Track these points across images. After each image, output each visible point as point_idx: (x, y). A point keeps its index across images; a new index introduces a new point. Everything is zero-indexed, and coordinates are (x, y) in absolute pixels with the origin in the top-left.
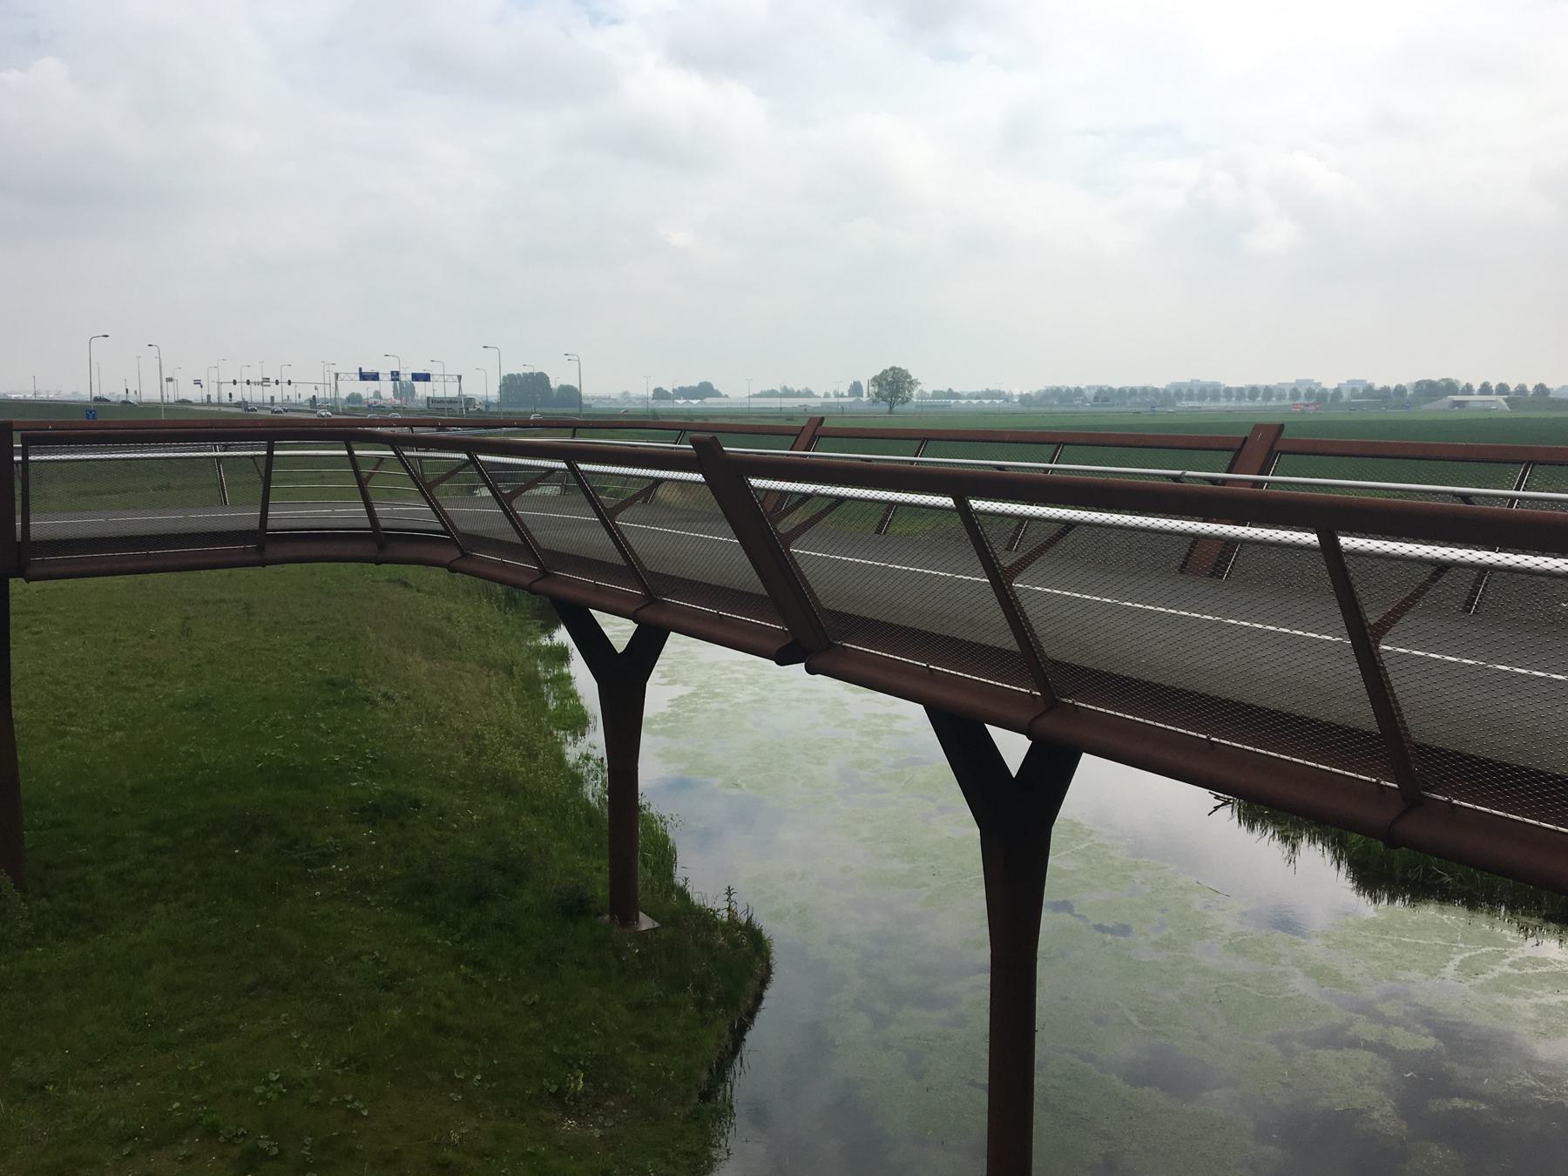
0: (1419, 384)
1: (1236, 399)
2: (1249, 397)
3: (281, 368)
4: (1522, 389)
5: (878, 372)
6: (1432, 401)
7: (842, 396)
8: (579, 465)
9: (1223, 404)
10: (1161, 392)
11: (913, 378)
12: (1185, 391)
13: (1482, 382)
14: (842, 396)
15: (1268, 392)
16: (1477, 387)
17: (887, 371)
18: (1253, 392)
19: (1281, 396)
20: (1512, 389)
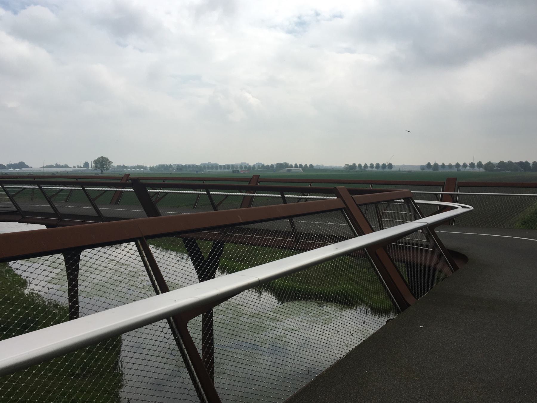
0: (277, 164)
7: (81, 167)
11: (110, 161)
12: (206, 166)
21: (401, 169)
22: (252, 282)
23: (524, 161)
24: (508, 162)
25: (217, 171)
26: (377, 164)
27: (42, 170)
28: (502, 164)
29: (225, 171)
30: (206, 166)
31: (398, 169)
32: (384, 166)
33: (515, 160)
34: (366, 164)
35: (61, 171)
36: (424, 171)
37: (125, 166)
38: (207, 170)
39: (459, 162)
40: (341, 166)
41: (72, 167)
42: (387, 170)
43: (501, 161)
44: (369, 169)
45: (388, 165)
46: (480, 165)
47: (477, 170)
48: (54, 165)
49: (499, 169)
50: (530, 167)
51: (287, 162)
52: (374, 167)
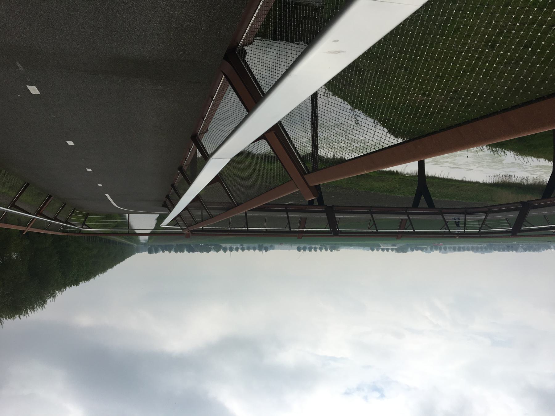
0: (406, 252)
1: (465, 247)
2: (461, 248)
4: (378, 250)
6: (402, 246)
8: (23, 234)
9: (470, 246)
10: (493, 250)
13: (389, 252)
15: (454, 249)
16: (390, 251)
18: (459, 250)
19: (450, 248)
20: (380, 250)
24: (203, 252)
26: (260, 251)
28: (208, 251)
31: (292, 246)
32: (305, 249)
36: (270, 245)
39: (242, 252)
42: (302, 246)
43: (189, 253)
44: (318, 246)
46: (225, 250)
47: (228, 246)
49: (210, 246)
50: (186, 248)
51: (397, 253)
52: (314, 248)
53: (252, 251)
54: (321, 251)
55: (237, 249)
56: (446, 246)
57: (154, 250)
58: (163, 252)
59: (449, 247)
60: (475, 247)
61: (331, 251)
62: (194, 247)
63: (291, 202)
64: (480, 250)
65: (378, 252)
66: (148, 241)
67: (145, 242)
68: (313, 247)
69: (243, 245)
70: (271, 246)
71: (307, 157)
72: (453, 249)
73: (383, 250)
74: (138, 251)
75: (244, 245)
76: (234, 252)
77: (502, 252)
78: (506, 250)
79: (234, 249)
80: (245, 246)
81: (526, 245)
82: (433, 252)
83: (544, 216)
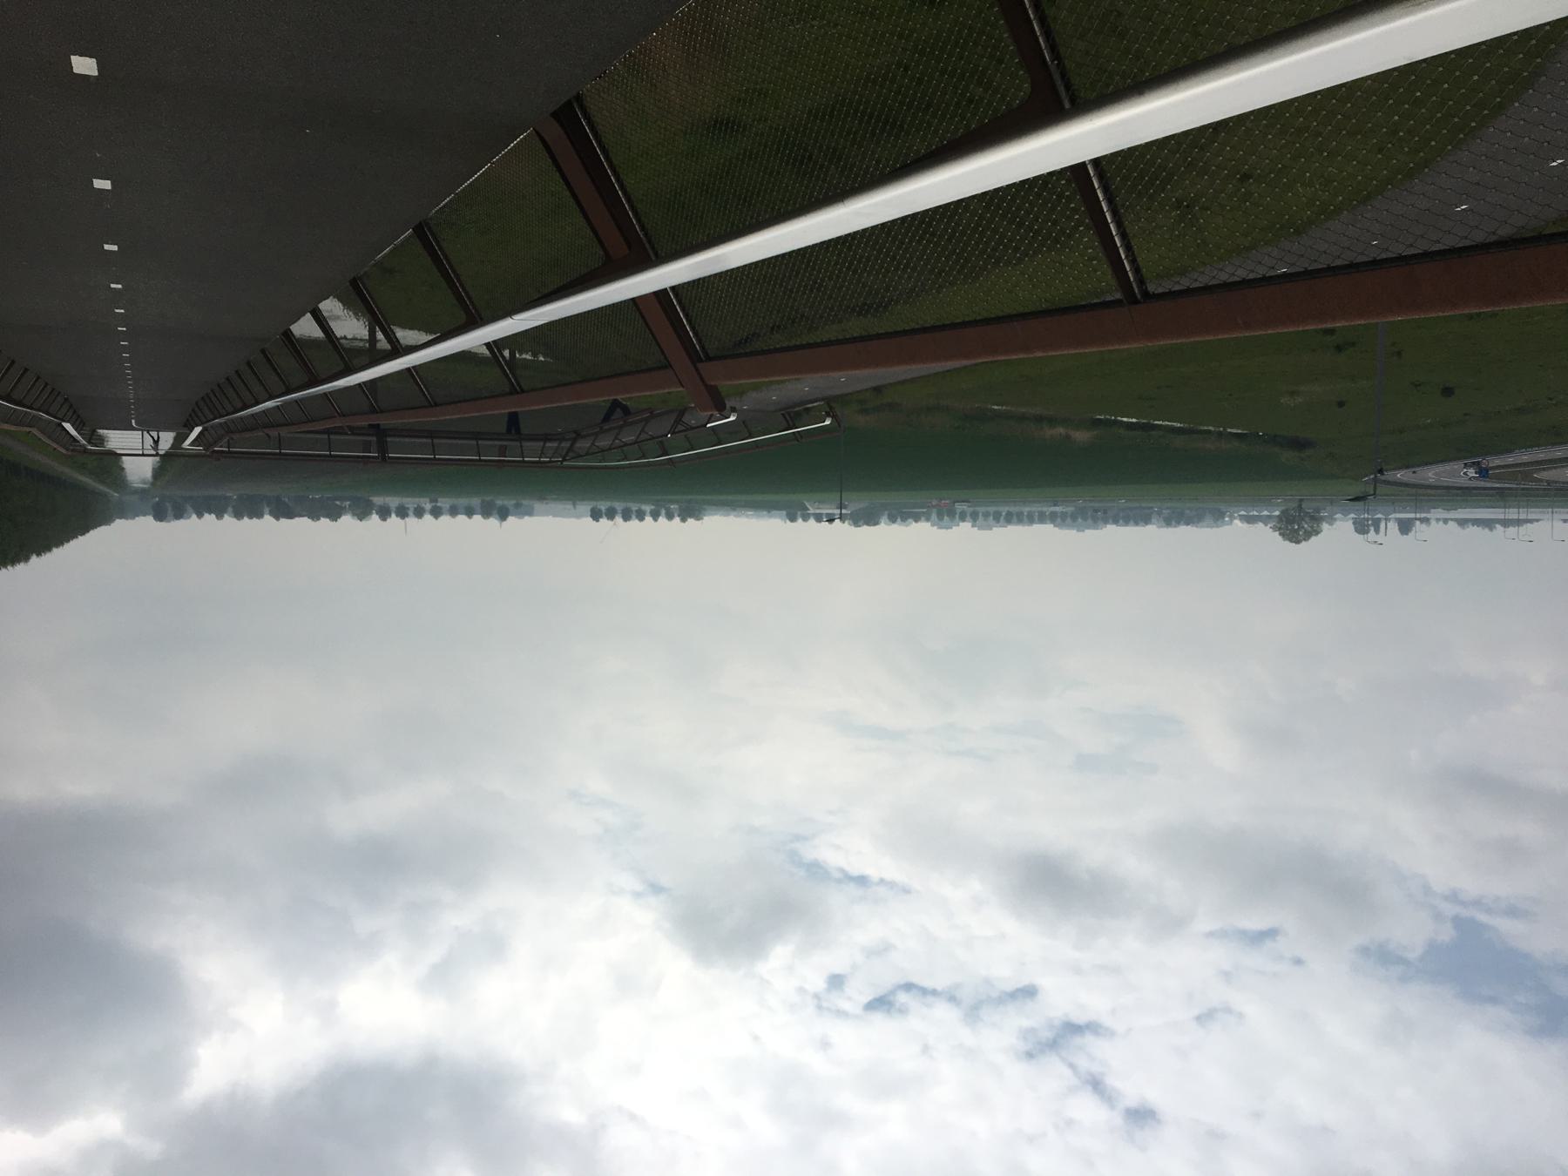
0: (876, 523)
3: (1418, 540)
5: (1313, 539)
7: (1420, 520)
11: (1277, 533)
12: (1069, 520)
14: (1420, 520)
17: (1305, 540)
18: (1009, 519)
19: (997, 517)
21: (569, 506)
22: (1116, 105)
23: (284, 520)
24: (319, 519)
25: (1040, 509)
27: (1533, 513)
28: (334, 515)
29: (608, 504)
30: (1069, 520)
31: (577, 507)
32: (611, 515)
33: (303, 522)
34: (655, 520)
35: (1463, 510)
37: (150, 519)
38: (1070, 509)
39: (434, 519)
40: (734, 518)
41: (1433, 522)
42: (603, 506)
43: (277, 519)
44: (647, 508)
45: (601, 517)
46: (384, 513)
47: (393, 502)
48: (1497, 526)
49: (338, 503)
50: (268, 506)
51: (853, 527)
52: (637, 511)
53: (462, 518)
54: (655, 520)
55: (419, 513)
56: (978, 509)
57: (170, 508)
58: (200, 515)
59: (983, 513)
60: (1047, 514)
61: (684, 520)
62: (290, 505)
63: (996, 407)
64: (1059, 520)
65: (805, 523)
66: (153, 484)
67: (141, 485)
68: (600, 511)
69: (437, 501)
70: (518, 506)
71: (731, 277)
72: (994, 519)
73: (819, 518)
74: (125, 512)
75: (439, 500)
76: (412, 521)
77: (1175, 527)
78: (1121, 521)
79: (411, 513)
80: (444, 503)
81: (1168, 508)
82: (958, 525)
83: (296, 402)
